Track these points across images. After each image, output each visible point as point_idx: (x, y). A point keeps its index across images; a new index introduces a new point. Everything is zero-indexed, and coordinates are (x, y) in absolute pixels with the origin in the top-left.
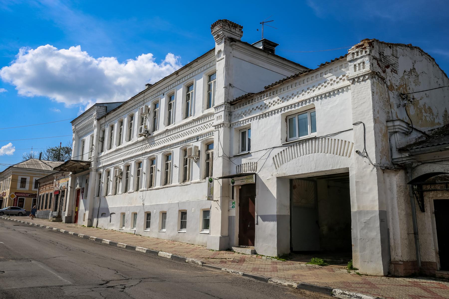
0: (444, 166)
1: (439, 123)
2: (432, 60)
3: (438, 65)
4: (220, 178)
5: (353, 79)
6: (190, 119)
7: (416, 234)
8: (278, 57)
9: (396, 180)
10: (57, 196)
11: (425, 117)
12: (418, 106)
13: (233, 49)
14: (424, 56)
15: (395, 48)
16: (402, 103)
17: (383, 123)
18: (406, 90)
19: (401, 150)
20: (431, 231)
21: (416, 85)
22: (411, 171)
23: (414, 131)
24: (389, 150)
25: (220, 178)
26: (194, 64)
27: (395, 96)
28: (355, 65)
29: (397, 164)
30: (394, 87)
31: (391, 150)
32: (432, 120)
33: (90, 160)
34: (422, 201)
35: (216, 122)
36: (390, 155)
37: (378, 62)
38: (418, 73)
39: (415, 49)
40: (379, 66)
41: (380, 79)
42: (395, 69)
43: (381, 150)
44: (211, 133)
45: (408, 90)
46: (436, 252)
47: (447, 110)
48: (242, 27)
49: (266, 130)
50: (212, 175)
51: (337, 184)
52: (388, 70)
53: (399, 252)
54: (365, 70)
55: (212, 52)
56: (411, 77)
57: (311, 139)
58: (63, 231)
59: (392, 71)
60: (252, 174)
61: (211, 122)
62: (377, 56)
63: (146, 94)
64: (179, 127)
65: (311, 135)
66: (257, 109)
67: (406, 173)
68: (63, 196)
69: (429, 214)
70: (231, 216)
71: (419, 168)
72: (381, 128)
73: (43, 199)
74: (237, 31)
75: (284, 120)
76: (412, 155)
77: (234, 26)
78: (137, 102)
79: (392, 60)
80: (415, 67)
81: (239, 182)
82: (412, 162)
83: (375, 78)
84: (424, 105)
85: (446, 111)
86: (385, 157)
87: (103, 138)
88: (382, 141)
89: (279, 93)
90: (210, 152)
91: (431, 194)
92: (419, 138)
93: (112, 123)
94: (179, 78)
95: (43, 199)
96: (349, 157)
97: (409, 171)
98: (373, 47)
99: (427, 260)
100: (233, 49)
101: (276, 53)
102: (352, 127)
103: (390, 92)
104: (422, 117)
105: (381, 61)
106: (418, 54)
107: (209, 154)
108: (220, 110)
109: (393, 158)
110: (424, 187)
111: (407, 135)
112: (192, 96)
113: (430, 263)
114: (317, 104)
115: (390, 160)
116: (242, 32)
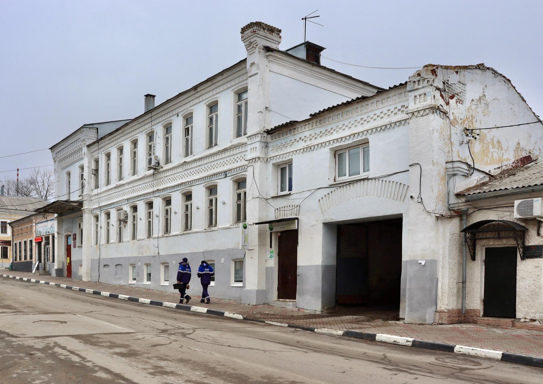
0: (499, 212)
1: (508, 159)
2: (507, 82)
3: (514, 88)
4: (256, 224)
5: (413, 113)
6: (214, 150)
7: (464, 282)
8: (324, 68)
9: (453, 227)
10: (39, 244)
11: (492, 153)
12: (485, 141)
13: (269, 61)
14: (497, 78)
15: (463, 72)
16: (466, 139)
17: (442, 165)
18: (472, 123)
19: (458, 195)
20: (479, 280)
21: (484, 115)
22: (467, 218)
23: (475, 172)
24: (447, 194)
25: (256, 224)
26: (218, 78)
27: (458, 132)
28: (416, 96)
29: (454, 210)
30: (457, 122)
31: (448, 195)
32: (501, 155)
33: (81, 197)
34: (474, 249)
35: (250, 156)
36: (447, 201)
37: (441, 93)
38: (489, 101)
39: (488, 70)
40: (443, 97)
41: (442, 113)
42: (461, 98)
43: (437, 195)
44: (244, 168)
45: (474, 123)
46: (481, 301)
47: (520, 142)
48: (280, 31)
49: (312, 164)
50: (245, 219)
51: (390, 229)
52: (452, 102)
53: (445, 301)
54: (426, 103)
55: (243, 66)
56: (479, 107)
57: (364, 180)
58: (11, 276)
59: (457, 102)
60: (294, 219)
61: (243, 155)
62: (441, 86)
63: (153, 113)
64: (200, 159)
65: (363, 175)
66: (301, 141)
67: (461, 220)
68: (47, 243)
69: (480, 262)
70: (269, 267)
71: (474, 214)
72: (439, 170)
73: (20, 248)
74: (274, 36)
75: (333, 156)
76: (468, 201)
77: (271, 30)
78: (142, 124)
79: (457, 89)
80: (485, 94)
81: (278, 228)
82: (468, 208)
83: (436, 112)
84: (492, 140)
85: (519, 144)
86: (441, 203)
87: (97, 170)
88: (439, 185)
89: (327, 123)
90: (214, 115)
91: (484, 242)
92: (482, 179)
93: (107, 151)
94: (198, 94)
95: (20, 248)
96: (403, 201)
97: (464, 217)
98: (436, 75)
99: (472, 308)
100: (269, 61)
101: (322, 63)
102: (407, 168)
103: (452, 127)
104: (489, 153)
105: (445, 90)
106: (490, 77)
107: (240, 194)
108: (255, 141)
109: (450, 203)
110: (477, 237)
111: (468, 177)
112: (298, 345)
113: (474, 311)
114: (372, 139)
115: (447, 205)
116: (280, 37)
